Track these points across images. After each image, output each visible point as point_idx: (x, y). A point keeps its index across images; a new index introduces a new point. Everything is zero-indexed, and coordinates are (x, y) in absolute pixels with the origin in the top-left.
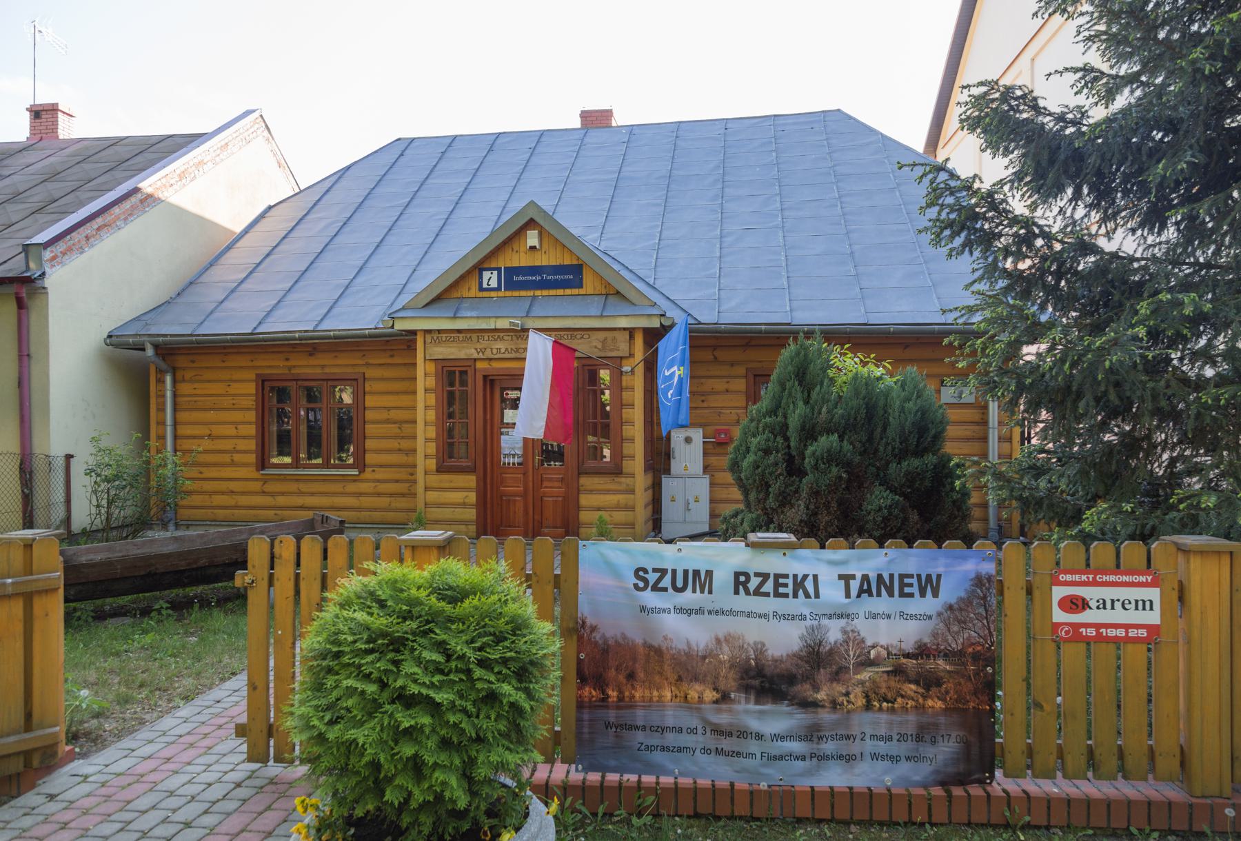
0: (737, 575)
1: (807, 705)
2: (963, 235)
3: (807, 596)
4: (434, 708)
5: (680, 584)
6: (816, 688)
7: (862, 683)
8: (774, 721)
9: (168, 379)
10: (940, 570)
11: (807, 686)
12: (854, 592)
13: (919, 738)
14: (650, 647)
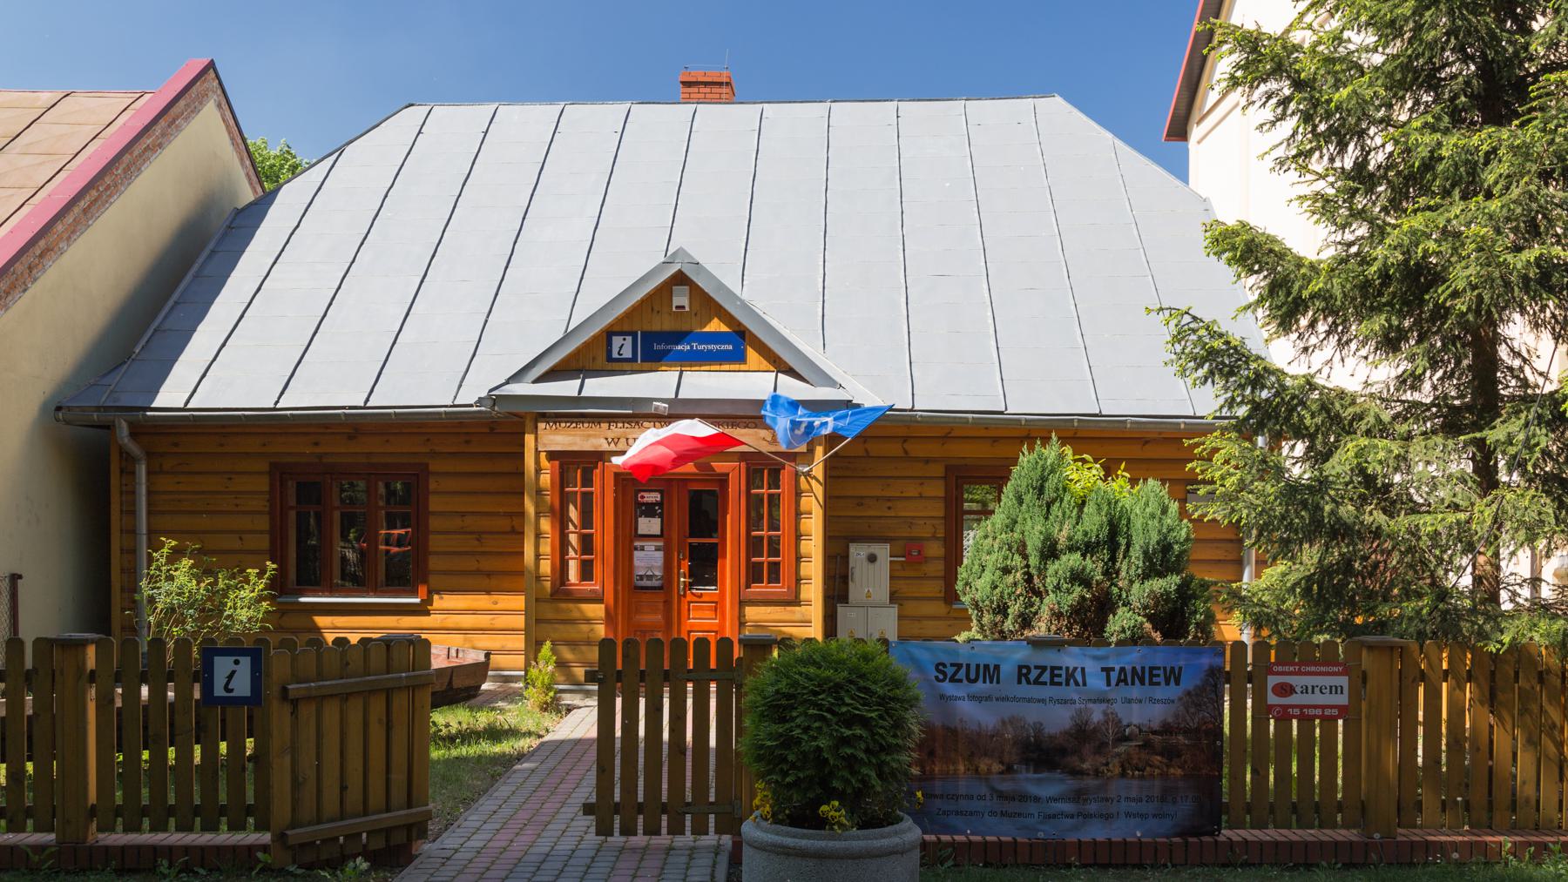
0: (1020, 668)
1: (1076, 773)
2: (1207, 365)
3: (1077, 684)
4: (864, 722)
5: (973, 676)
6: (1083, 760)
7: (1118, 755)
8: (1048, 787)
9: (142, 470)
10: (1181, 663)
11: (1075, 758)
12: (1113, 682)
13: (1163, 799)
14: (948, 728)
